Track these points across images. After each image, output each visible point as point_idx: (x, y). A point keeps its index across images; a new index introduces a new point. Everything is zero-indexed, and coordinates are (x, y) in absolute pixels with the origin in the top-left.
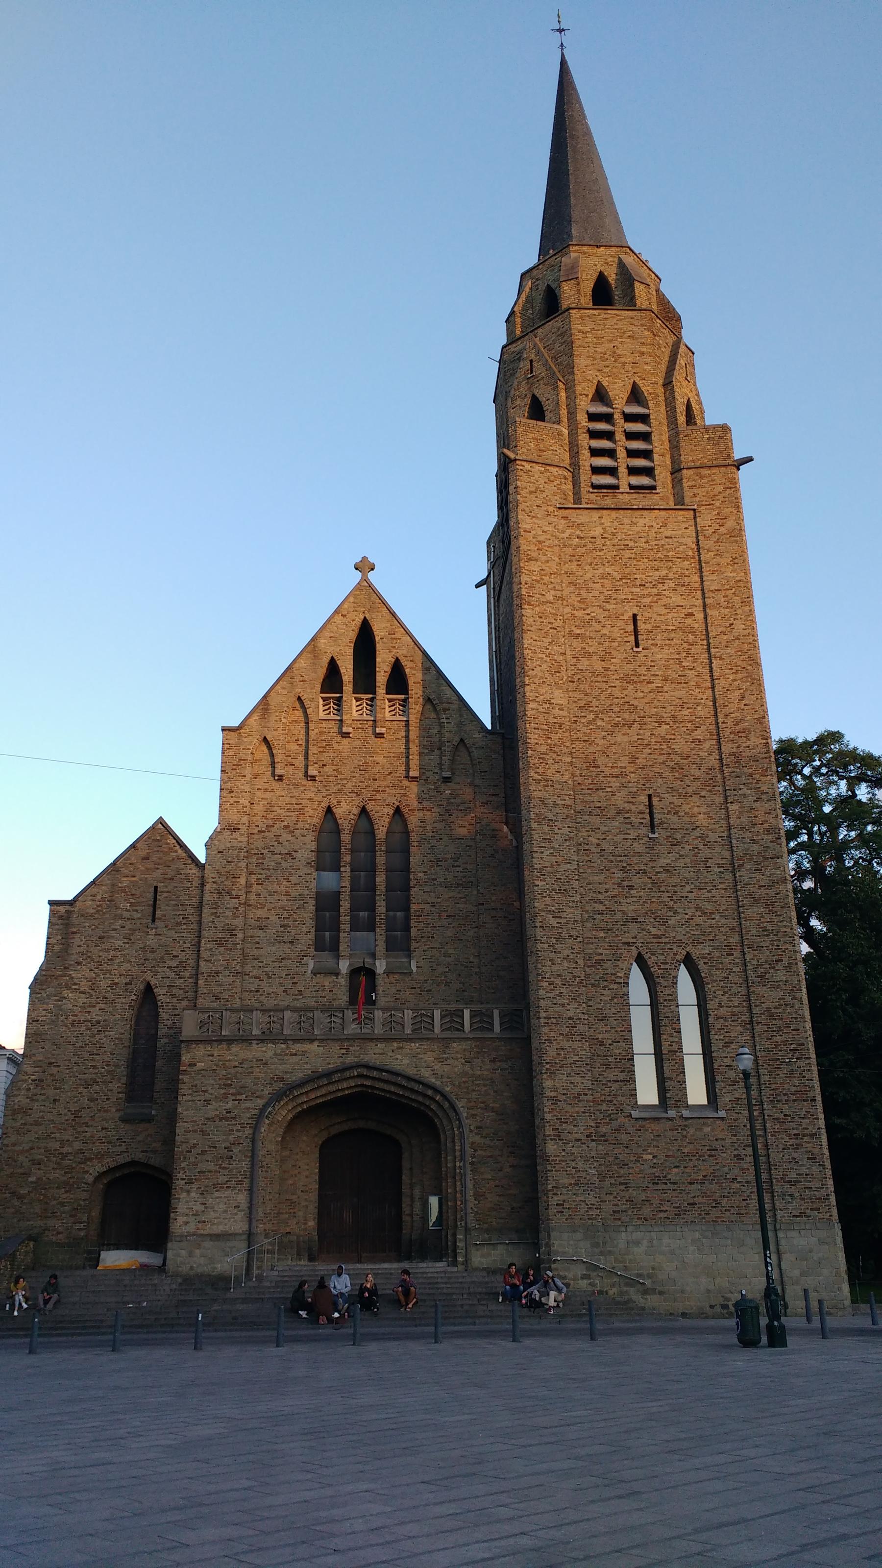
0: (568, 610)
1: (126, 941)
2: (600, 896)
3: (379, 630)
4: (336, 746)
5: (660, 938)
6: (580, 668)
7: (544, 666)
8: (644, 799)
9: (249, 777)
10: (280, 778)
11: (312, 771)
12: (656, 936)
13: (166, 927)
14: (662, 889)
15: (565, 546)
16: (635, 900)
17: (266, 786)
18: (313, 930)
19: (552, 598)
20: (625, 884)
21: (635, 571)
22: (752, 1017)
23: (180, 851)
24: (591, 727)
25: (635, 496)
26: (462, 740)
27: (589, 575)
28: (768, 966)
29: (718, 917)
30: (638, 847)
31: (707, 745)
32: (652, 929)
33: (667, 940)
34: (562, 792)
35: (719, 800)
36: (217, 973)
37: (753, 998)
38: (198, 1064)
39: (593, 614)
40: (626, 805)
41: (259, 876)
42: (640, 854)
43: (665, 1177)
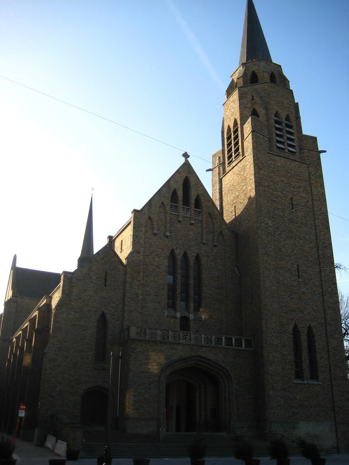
0: (271, 191)
1: (95, 293)
2: (283, 300)
3: (192, 182)
4: (175, 225)
5: (302, 318)
6: (276, 213)
7: (266, 210)
8: (296, 266)
9: (144, 231)
10: (155, 235)
11: (168, 234)
12: (300, 317)
13: (111, 289)
14: (302, 300)
15: (269, 167)
16: (294, 303)
17: (149, 236)
18: (167, 299)
19: (267, 185)
20: (291, 297)
21: (291, 182)
22: (328, 349)
23: (116, 258)
24: (279, 236)
25: (290, 154)
26: (221, 232)
27: (277, 180)
28: (333, 332)
29: (318, 312)
30: (295, 284)
31: (314, 250)
32: (299, 315)
33: (304, 319)
34: (272, 259)
35: (318, 270)
36: (132, 311)
37: (329, 342)
38: (137, 349)
39: (279, 194)
40: (291, 267)
41: (147, 274)
42: (295, 286)
43: (303, 404)
